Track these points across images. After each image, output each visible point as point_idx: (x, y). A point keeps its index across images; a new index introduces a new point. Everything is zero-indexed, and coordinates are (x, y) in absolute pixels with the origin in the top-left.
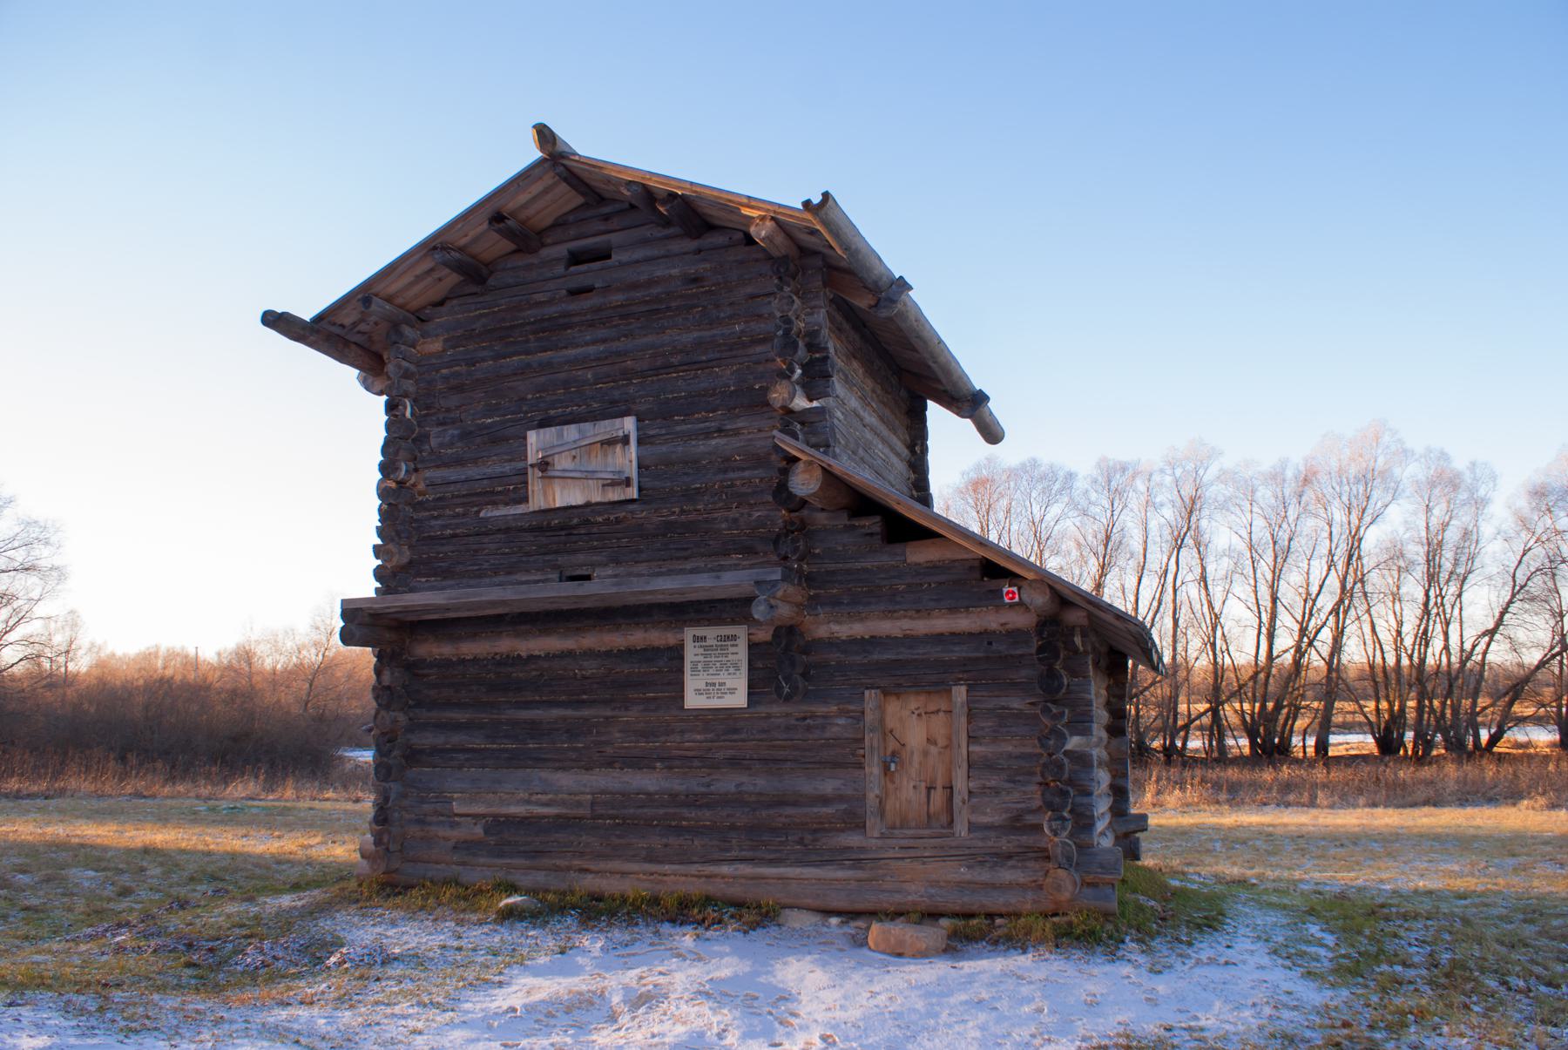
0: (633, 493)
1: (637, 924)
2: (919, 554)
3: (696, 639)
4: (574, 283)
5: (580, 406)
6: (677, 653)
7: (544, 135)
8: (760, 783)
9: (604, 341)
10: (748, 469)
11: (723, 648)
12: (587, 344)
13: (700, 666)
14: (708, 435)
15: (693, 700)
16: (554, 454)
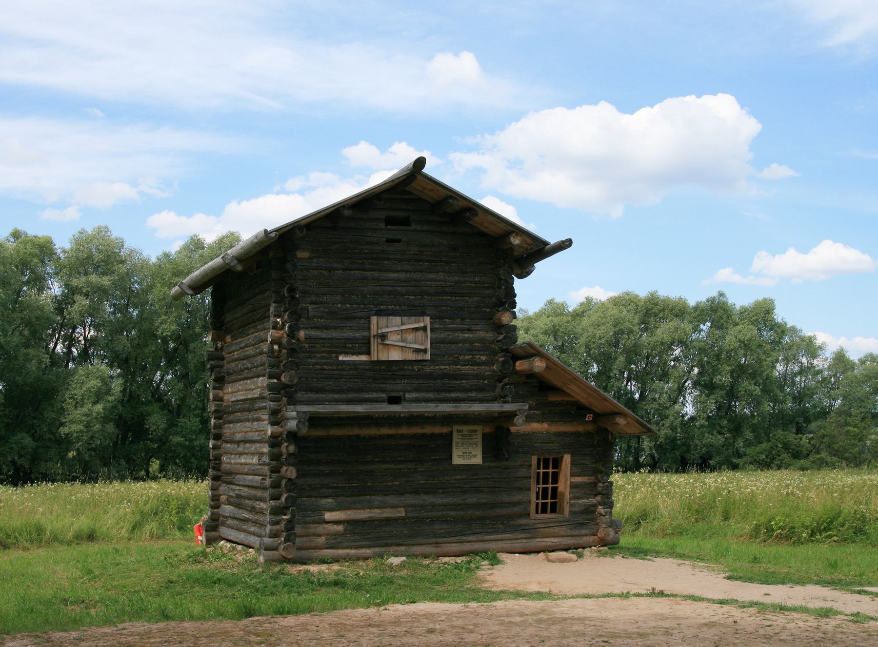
0: (428, 357)
1: (5, 571)
2: (553, 398)
3: (458, 431)
4: (389, 236)
5: (395, 306)
6: (450, 435)
8: (484, 498)
9: (407, 272)
10: (481, 351)
11: (471, 436)
12: (398, 271)
13: (459, 444)
14: (462, 330)
15: (457, 460)
16: (388, 332)
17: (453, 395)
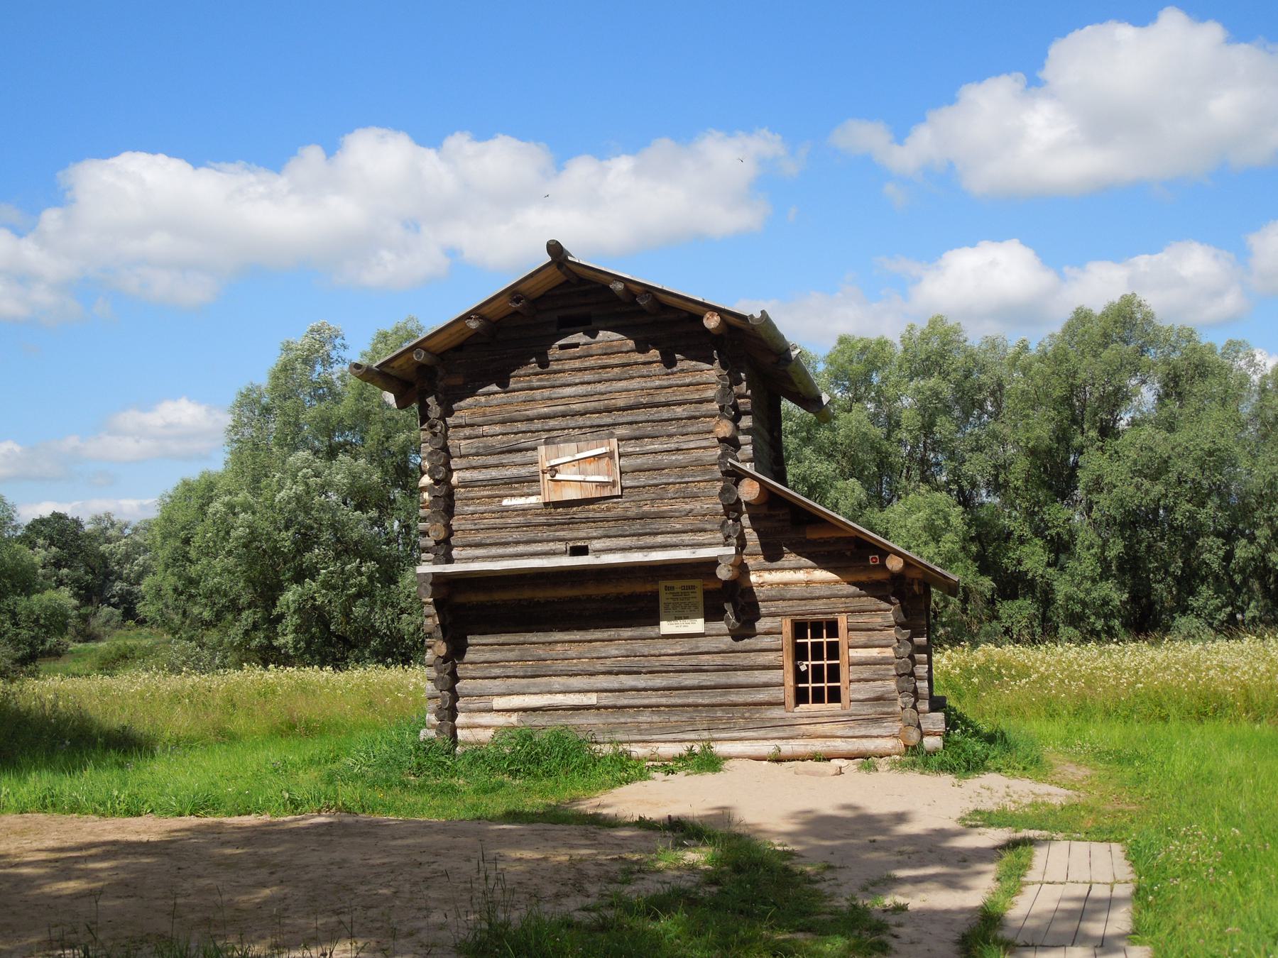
2: (813, 534)
3: (667, 588)
6: (655, 597)
13: (670, 606)
16: (558, 465)
17: (660, 539)
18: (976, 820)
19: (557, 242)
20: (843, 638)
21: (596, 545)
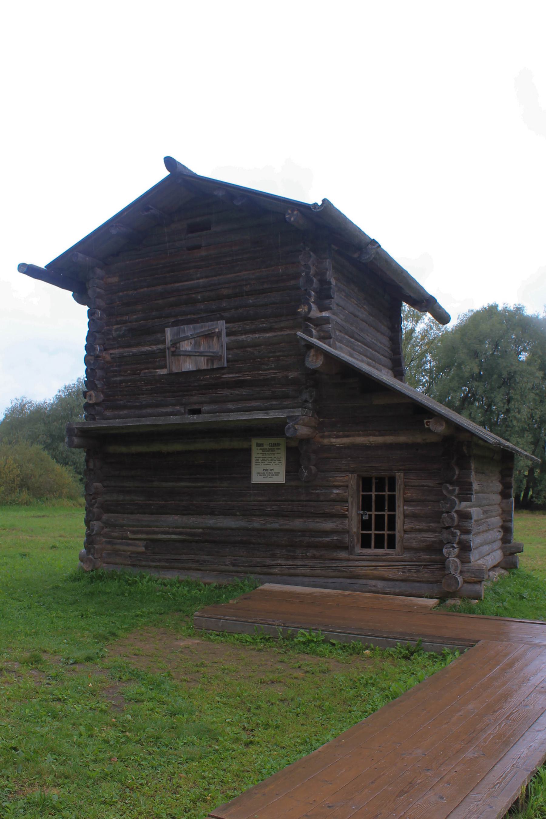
6: (248, 451)
7: (169, 162)
13: (260, 460)
15: (256, 479)
18: (512, 729)
19: (450, 320)
20: (399, 494)
21: (205, 408)
